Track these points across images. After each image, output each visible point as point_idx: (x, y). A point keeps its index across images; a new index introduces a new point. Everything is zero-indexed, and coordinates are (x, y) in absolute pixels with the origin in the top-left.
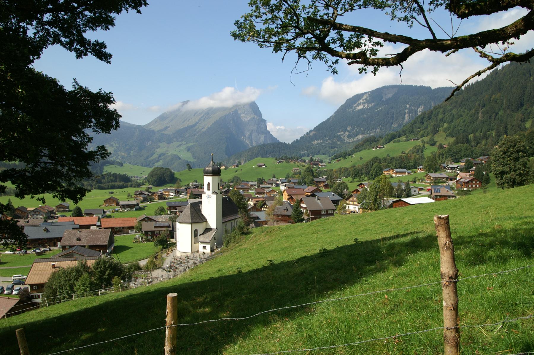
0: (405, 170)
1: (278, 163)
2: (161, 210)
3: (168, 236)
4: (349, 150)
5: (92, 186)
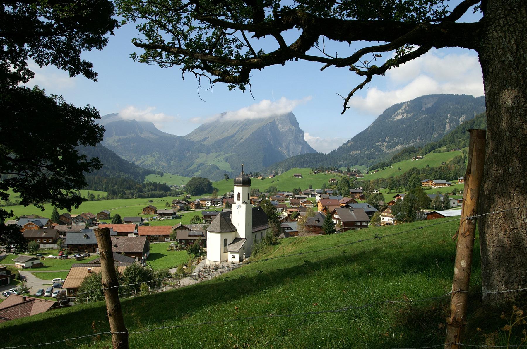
0: (444, 181)
1: (315, 173)
2: (197, 220)
3: (201, 245)
4: (387, 161)
5: (133, 194)
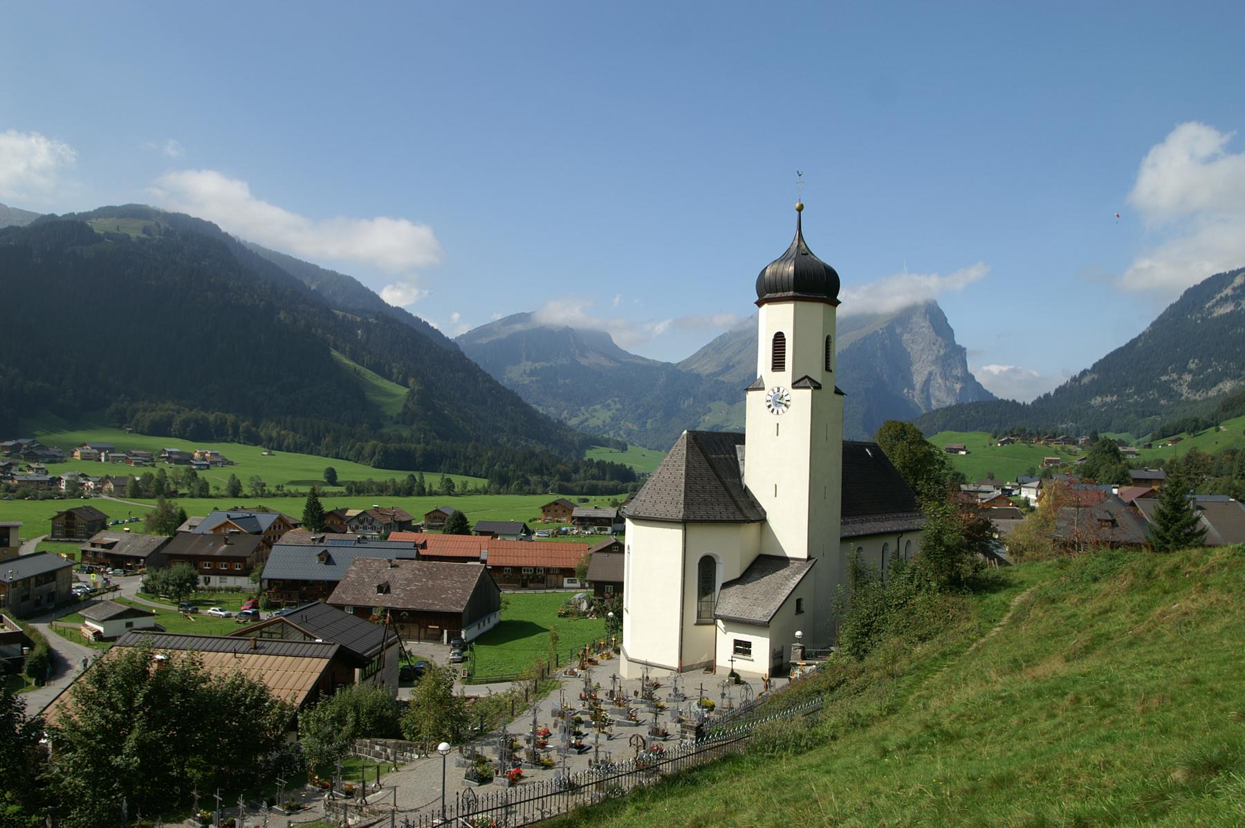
5: (546, 485)
